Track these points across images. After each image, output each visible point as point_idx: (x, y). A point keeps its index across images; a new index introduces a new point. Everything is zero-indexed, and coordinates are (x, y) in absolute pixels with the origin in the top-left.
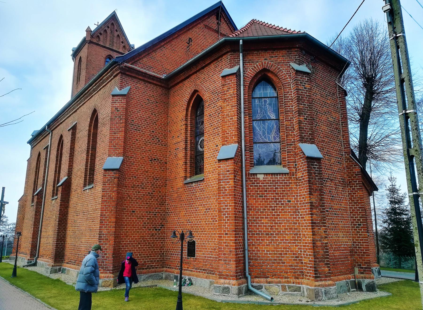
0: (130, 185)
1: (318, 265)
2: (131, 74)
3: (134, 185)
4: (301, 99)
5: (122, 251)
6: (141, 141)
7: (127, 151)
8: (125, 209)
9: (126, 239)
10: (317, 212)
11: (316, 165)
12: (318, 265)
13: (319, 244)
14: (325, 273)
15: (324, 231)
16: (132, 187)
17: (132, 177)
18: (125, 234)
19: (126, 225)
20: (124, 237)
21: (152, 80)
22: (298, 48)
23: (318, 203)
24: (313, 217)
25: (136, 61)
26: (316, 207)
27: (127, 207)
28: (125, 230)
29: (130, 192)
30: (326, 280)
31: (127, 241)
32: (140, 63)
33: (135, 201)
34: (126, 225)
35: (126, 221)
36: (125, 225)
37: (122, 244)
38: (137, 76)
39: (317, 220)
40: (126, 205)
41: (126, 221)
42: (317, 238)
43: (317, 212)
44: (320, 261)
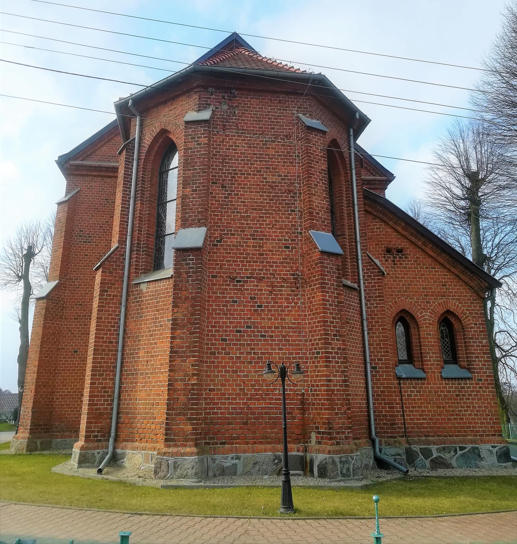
0: (73, 316)
1: (174, 419)
2: (81, 173)
3: (78, 316)
4: (190, 163)
5: (56, 405)
6: (92, 256)
7: (71, 271)
8: (64, 349)
9: (63, 389)
10: (184, 333)
11: (190, 260)
12: (174, 419)
13: (179, 385)
14: (184, 433)
15: (192, 365)
16: (75, 319)
17: (77, 305)
18: (61, 382)
19: (64, 370)
20: (60, 386)
21: (112, 173)
22: (197, 87)
23: (188, 319)
24: (174, 343)
25: (91, 154)
26: (182, 327)
27: (67, 346)
28: (62, 376)
29: (72, 325)
30: (185, 446)
31: (64, 392)
32: (96, 155)
33: (79, 337)
34: (64, 370)
35: (65, 364)
36: (63, 370)
37: (56, 395)
38: (89, 173)
39: (182, 347)
40: (65, 342)
41: (65, 364)
42: (179, 376)
43: (184, 333)
44: (177, 414)
